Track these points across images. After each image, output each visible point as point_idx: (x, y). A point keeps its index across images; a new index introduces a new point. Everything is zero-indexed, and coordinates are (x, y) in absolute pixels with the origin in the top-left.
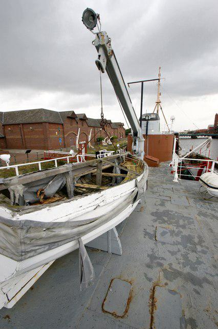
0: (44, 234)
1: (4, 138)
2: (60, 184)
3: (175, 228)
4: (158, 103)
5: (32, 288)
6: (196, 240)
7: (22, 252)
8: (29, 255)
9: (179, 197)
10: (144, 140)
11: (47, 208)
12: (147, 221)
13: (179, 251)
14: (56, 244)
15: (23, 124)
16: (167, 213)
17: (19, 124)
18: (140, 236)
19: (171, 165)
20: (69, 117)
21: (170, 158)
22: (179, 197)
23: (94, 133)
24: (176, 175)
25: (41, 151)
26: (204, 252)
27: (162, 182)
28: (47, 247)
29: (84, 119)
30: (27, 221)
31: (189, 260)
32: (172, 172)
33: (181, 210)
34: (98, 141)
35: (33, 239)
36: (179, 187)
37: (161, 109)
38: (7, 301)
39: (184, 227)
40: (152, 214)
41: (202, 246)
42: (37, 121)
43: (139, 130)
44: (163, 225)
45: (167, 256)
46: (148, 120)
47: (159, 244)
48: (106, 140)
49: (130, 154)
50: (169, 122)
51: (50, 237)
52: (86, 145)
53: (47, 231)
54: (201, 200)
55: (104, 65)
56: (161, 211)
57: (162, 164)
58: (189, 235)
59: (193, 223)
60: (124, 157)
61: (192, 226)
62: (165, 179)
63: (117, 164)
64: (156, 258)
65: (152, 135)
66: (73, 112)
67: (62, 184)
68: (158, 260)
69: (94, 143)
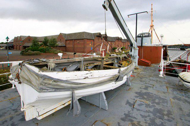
0: (51, 82)
1: (65, 46)
2: (76, 67)
3: (150, 103)
4: (152, 26)
5: (53, 114)
6: (166, 113)
7: (41, 88)
8: (44, 91)
9: (160, 86)
10: (138, 49)
11: (57, 72)
12: (130, 96)
13: (149, 116)
14: (59, 90)
15: (74, 40)
16: (148, 94)
17: (73, 40)
18: (123, 103)
19: (160, 66)
20: (97, 36)
21: (159, 62)
22: (160, 86)
23: (111, 46)
24: (162, 72)
25: (82, 54)
26: (169, 120)
27: (150, 76)
28: (54, 90)
29: (106, 37)
30: (44, 75)
31: (155, 123)
32: (160, 71)
33: (160, 94)
34: (113, 50)
35: (46, 84)
36: (162, 80)
37: (154, 30)
38: (38, 116)
39: (158, 104)
40: (136, 93)
41: (168, 117)
42: (81, 38)
43: (134, 43)
44: (142, 100)
45: (139, 118)
46: (143, 37)
47: (135, 110)
48: (118, 50)
49: (126, 56)
50: (160, 38)
51: (55, 85)
52: (105, 51)
53: (54, 82)
54: (179, 90)
55: (107, 7)
56: (143, 92)
57: (153, 65)
58: (161, 109)
59: (167, 102)
60: (121, 58)
61: (165, 104)
62: (153, 74)
63: (116, 62)
64: (130, 116)
65: (146, 46)
66: (100, 33)
67: (77, 67)
68: (131, 118)
69: (111, 51)
